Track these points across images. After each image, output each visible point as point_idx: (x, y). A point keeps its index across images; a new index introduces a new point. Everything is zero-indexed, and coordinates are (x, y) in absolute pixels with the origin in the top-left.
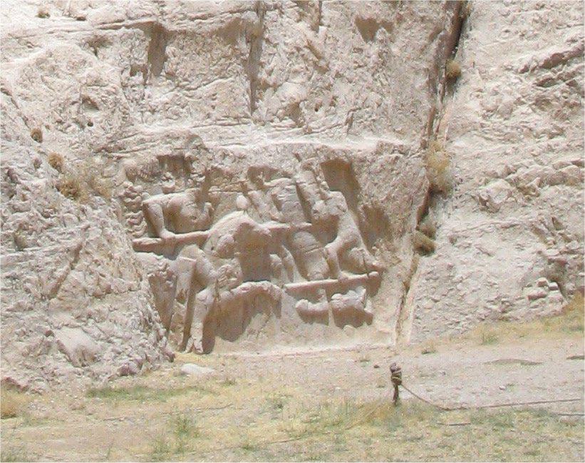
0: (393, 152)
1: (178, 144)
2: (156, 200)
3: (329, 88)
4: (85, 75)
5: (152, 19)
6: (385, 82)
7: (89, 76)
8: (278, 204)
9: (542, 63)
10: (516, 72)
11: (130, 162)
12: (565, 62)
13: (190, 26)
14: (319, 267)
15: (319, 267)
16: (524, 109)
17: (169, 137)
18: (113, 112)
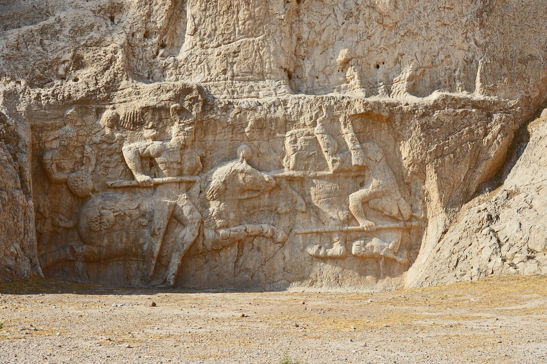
6: (481, 41)
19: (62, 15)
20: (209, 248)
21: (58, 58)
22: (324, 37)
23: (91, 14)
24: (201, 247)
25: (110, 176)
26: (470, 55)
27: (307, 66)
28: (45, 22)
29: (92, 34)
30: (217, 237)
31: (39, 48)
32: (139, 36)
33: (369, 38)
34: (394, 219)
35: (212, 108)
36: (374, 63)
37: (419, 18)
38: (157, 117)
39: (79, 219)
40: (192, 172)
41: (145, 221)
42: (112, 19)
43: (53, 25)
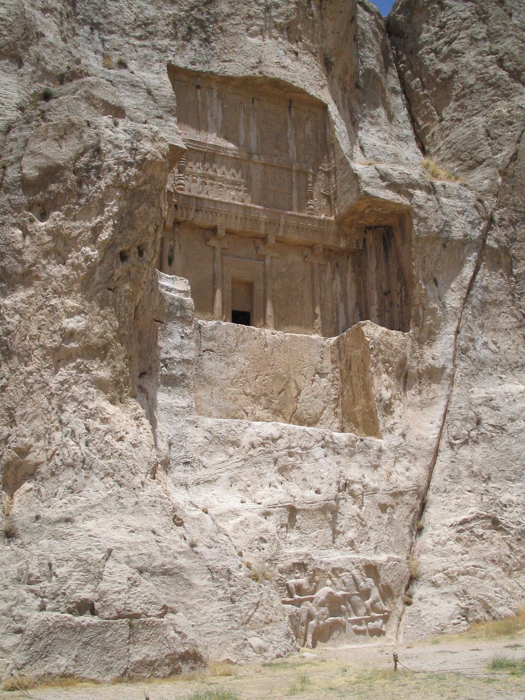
1: (301, 557)
2: (292, 582)
3: (366, 533)
11: (280, 565)
12: (468, 522)
13: (306, 506)
15: (362, 611)
16: (451, 542)
17: (297, 555)
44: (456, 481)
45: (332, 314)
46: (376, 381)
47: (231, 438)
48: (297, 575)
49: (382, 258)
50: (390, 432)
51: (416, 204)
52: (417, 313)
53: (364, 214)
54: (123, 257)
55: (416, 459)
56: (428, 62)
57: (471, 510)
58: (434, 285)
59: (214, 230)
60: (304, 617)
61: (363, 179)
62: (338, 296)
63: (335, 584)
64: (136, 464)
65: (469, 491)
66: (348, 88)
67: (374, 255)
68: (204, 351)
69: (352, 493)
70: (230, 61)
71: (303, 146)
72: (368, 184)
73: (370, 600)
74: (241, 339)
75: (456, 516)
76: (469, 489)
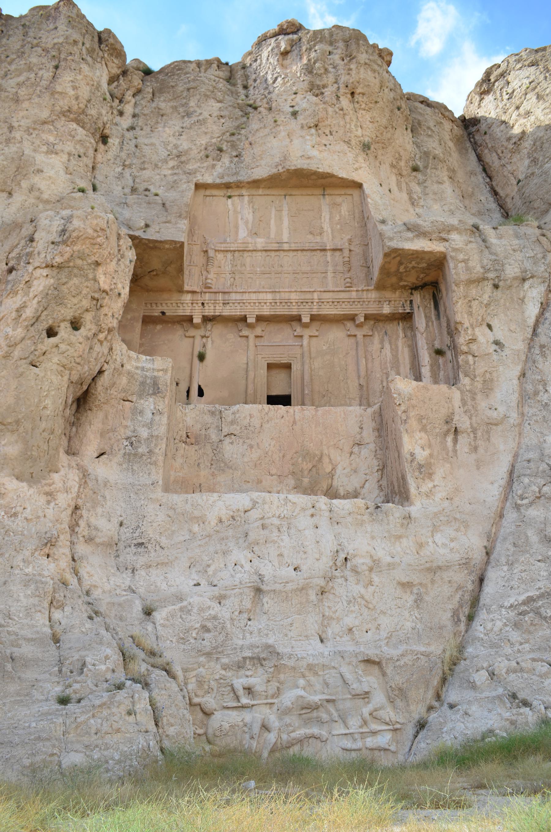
0: (416, 654)
1: (256, 651)
2: (239, 683)
3: (375, 619)
4: (207, 614)
5: (256, 584)
6: (418, 616)
7: (210, 614)
8: (327, 685)
9: (520, 602)
10: (506, 608)
11: (225, 660)
12: (534, 600)
13: (278, 587)
14: (354, 723)
15: (354, 723)
16: (507, 628)
17: (252, 647)
18: (220, 633)
19: (191, 600)
20: (284, 746)
21: (192, 626)
22: (337, 614)
23: (208, 600)
24: (279, 745)
25: (226, 700)
26: (414, 624)
27: (330, 632)
28: (181, 604)
29: (210, 612)
30: (289, 739)
31: (180, 620)
32: (236, 613)
33: (361, 615)
34: (387, 724)
35: (282, 658)
36: (365, 630)
37: (386, 604)
38: (252, 663)
39: (207, 728)
40: (273, 697)
41: (246, 729)
42: (220, 603)
43: (186, 607)
44: (522, 549)
45: (382, 384)
46: (406, 439)
47: (197, 513)
48: (249, 673)
49: (433, 317)
50: (427, 496)
51: (452, 248)
52: (467, 362)
53: (401, 273)
54: (51, 333)
55: (467, 527)
56: (499, 134)
57: (539, 584)
58: (487, 330)
59: (244, 319)
60: (256, 729)
61: (387, 236)
62: (388, 365)
63: (311, 685)
64: (24, 540)
65: (539, 561)
66: (405, 173)
67: (423, 315)
68: (226, 436)
69: (355, 570)
70: (257, 166)
71: (339, 226)
72: (391, 239)
73: (370, 707)
74: (266, 418)
75: (519, 594)
76: (540, 558)
